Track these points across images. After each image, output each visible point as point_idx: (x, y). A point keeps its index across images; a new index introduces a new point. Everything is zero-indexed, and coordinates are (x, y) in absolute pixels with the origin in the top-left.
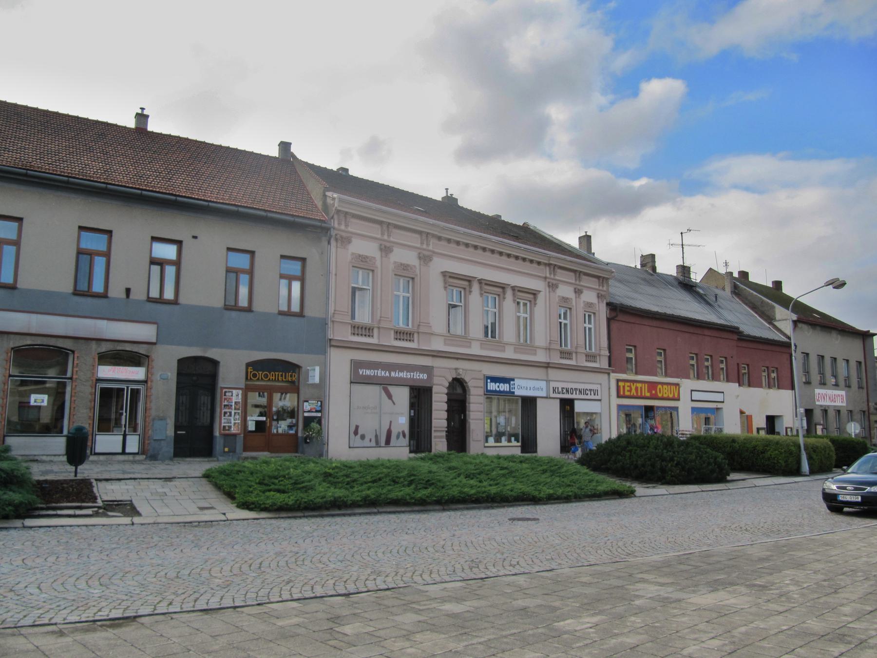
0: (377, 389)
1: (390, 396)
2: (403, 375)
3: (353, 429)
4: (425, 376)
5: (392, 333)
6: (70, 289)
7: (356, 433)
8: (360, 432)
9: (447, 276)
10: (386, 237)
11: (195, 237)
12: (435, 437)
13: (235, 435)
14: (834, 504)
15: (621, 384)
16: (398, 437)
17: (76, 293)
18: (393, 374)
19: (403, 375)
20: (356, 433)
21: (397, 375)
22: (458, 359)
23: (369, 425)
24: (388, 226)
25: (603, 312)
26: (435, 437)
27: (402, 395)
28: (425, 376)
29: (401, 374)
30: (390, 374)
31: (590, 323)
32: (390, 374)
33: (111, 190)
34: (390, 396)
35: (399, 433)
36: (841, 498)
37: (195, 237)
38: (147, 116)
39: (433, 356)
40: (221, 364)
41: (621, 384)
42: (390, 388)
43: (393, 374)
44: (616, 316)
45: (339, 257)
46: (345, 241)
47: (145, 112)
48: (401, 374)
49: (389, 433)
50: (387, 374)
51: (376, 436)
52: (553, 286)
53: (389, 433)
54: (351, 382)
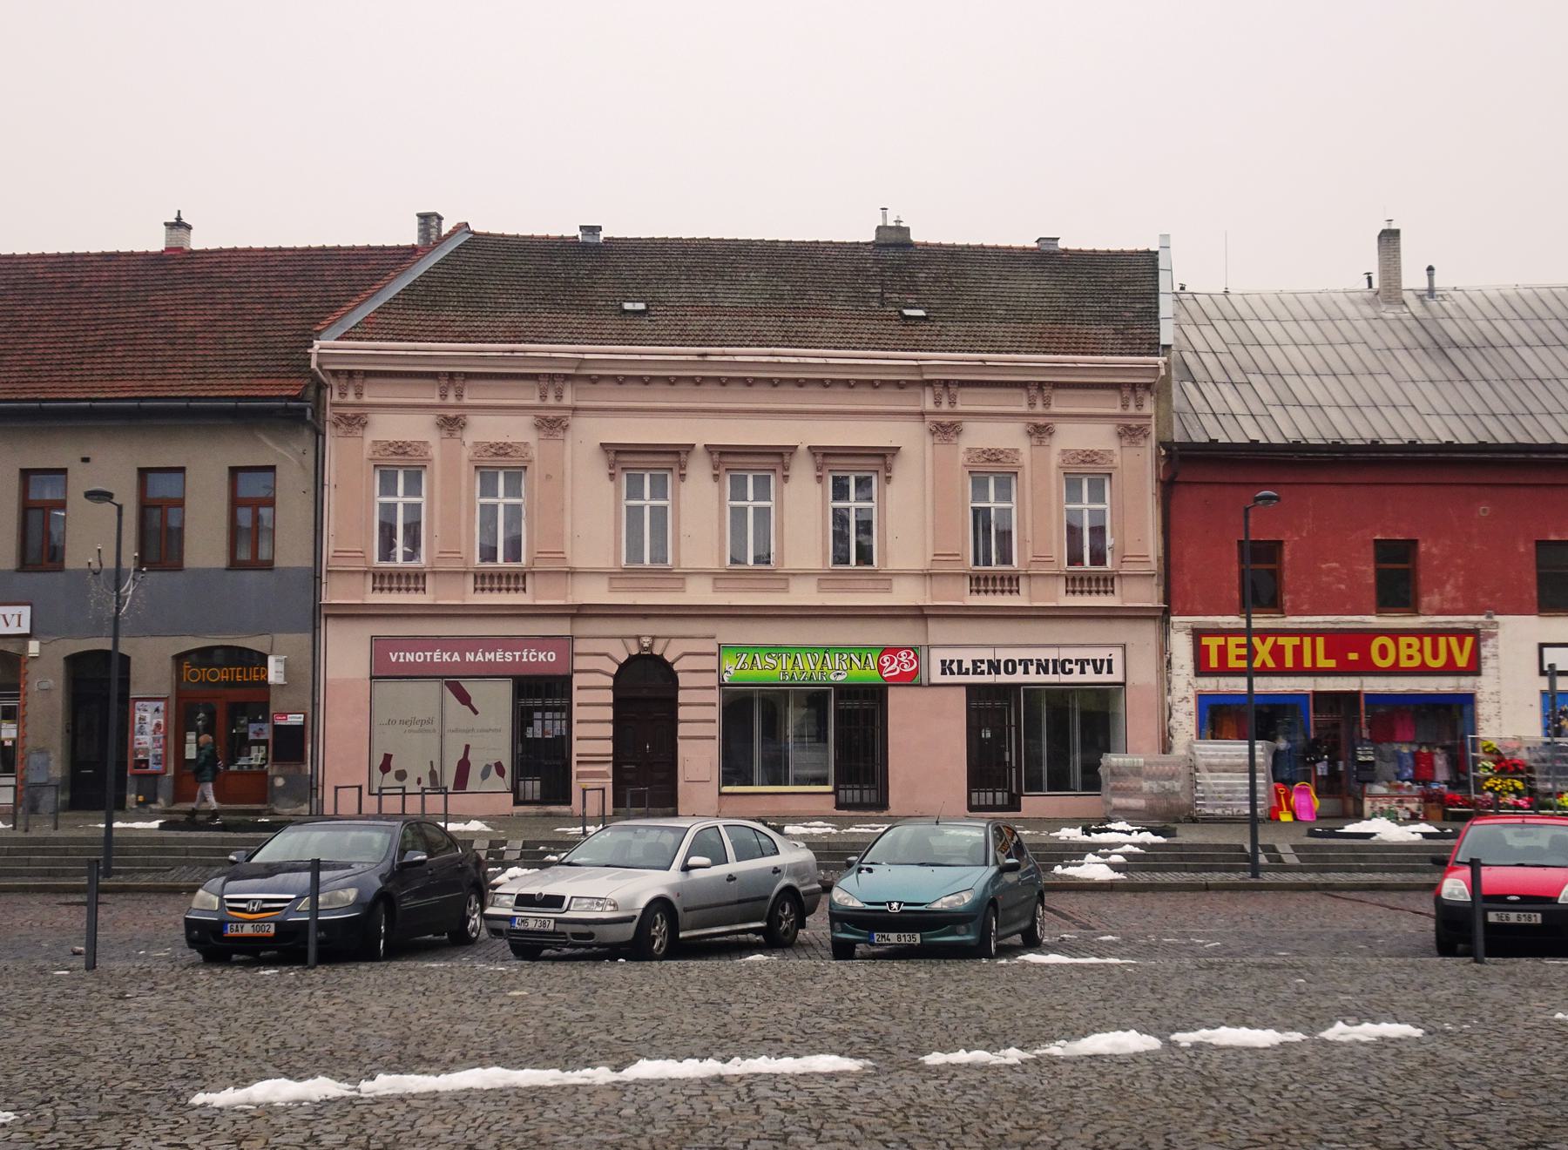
0: (434, 687)
1: (464, 698)
2: (497, 656)
3: (378, 760)
4: (552, 657)
5: (471, 579)
6: (222, 561)
7: (385, 767)
8: (395, 765)
9: (617, 454)
10: (551, 401)
11: (86, 460)
12: (580, 775)
13: (156, 775)
14: (213, 944)
15: (1213, 643)
16: (485, 774)
17: (235, 565)
18: (470, 657)
19: (497, 656)
20: (385, 767)
21: (480, 657)
22: (645, 617)
23: (415, 759)
24: (452, 379)
25: (1138, 470)
26: (580, 775)
27: (496, 700)
28: (552, 657)
29: (490, 656)
30: (463, 656)
31: (489, 512)
32: (463, 656)
33: (49, 409)
34: (464, 698)
35: (488, 767)
36: (230, 931)
37: (86, 460)
38: (1398, 232)
39: (573, 616)
40: (133, 660)
41: (1213, 643)
42: (468, 686)
43: (470, 657)
44: (1176, 475)
45: (345, 456)
46: (355, 422)
47: (1394, 227)
48: (490, 656)
49: (464, 768)
50: (456, 657)
51: (433, 774)
52: (946, 430)
53: (464, 768)
54: (1124, 684)
